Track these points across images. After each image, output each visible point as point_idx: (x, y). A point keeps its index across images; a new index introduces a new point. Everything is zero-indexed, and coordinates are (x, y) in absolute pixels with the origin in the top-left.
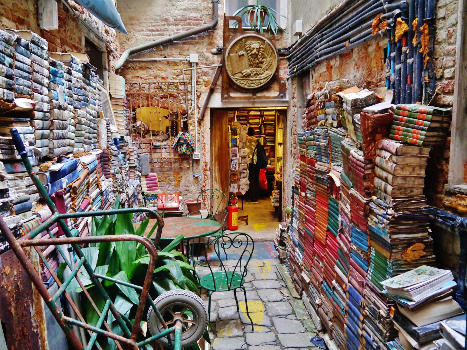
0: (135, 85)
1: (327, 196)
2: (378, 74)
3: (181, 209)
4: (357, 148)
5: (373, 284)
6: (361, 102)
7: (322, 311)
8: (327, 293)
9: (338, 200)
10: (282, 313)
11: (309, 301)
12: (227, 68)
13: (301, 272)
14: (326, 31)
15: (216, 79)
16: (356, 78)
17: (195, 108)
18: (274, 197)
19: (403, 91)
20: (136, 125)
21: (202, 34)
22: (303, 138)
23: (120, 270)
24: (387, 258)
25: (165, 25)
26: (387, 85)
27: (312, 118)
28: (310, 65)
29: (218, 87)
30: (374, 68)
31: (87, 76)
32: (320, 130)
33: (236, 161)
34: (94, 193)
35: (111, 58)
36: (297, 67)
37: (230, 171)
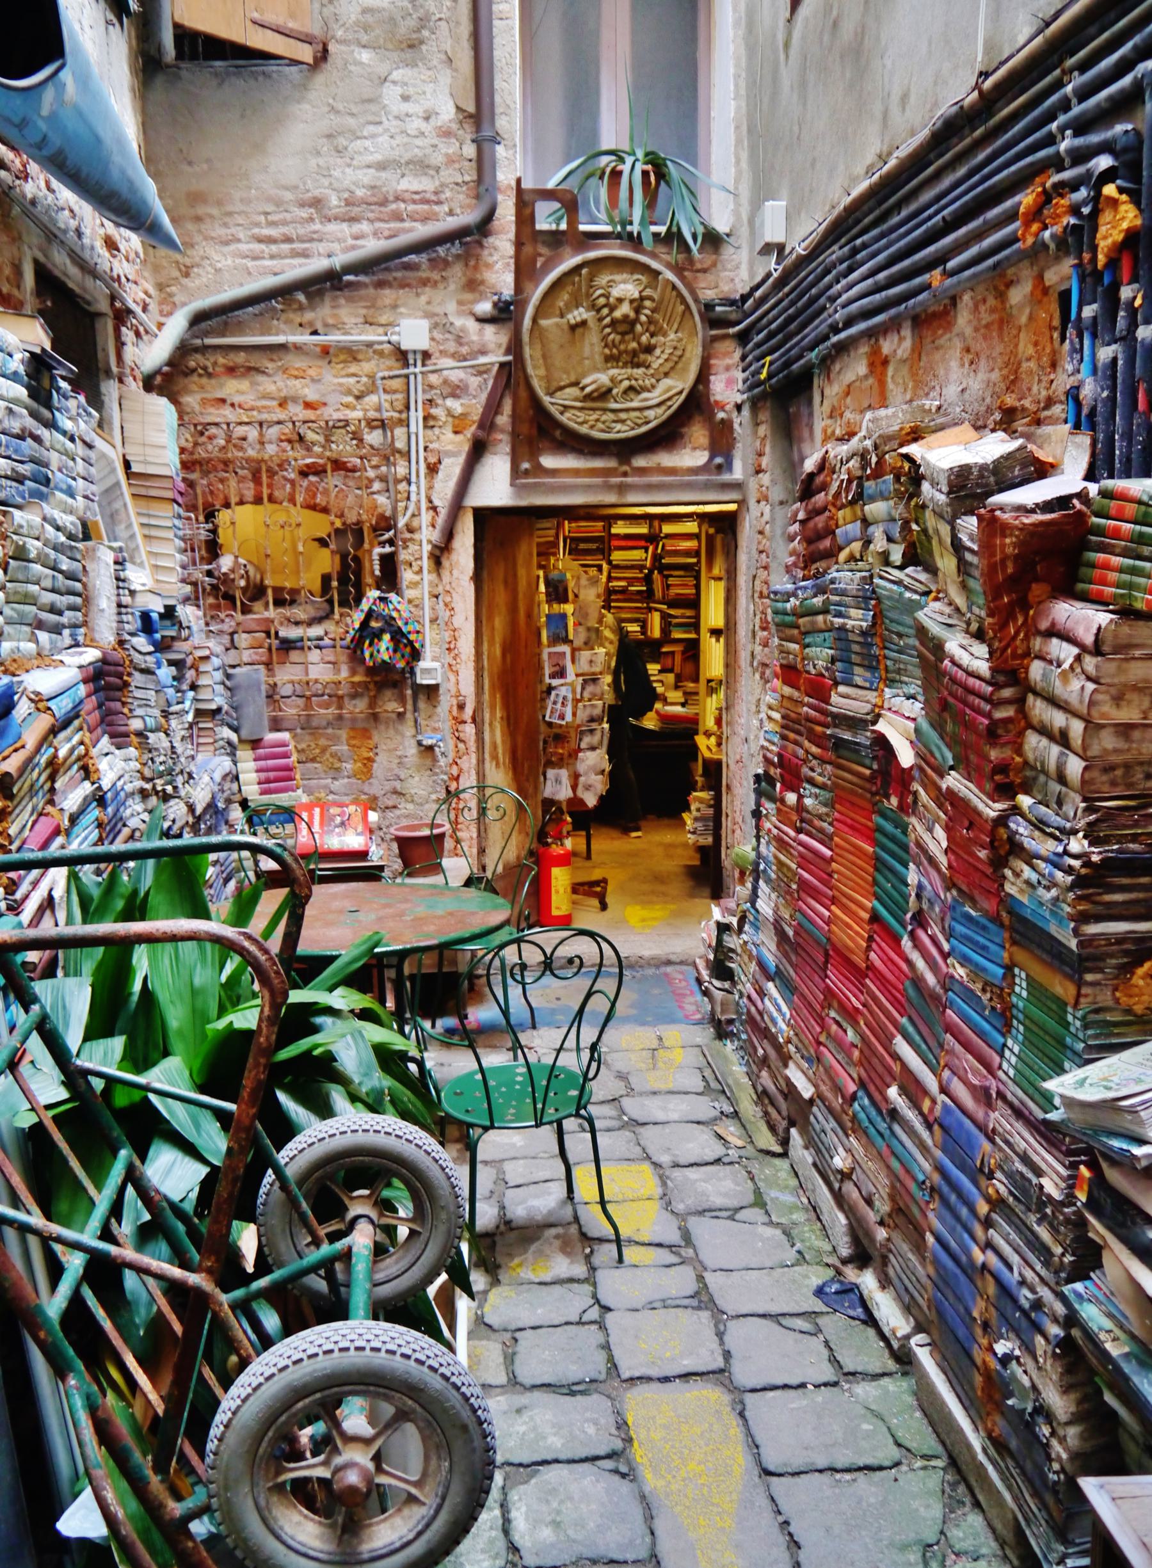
0: (213, 430)
1: (870, 801)
2: (1040, 381)
3: (377, 856)
4: (967, 632)
5: (1020, 1093)
6: (981, 476)
7: (855, 1194)
8: (872, 1130)
9: (908, 815)
10: (718, 1201)
11: (810, 1160)
12: (530, 370)
13: (786, 1066)
14: (865, 238)
15: (492, 407)
16: (966, 395)
17: (419, 509)
18: (695, 813)
19: (1122, 436)
20: (219, 567)
21: (441, 251)
22: (788, 606)
23: (166, 1053)
24: (1066, 1004)
25: (311, 219)
26: (1071, 417)
27: (819, 536)
28: (814, 354)
29: (500, 436)
30: (1029, 359)
31: (43, 393)
32: (844, 577)
33: (563, 691)
34: (73, 796)
35: (128, 335)
36: (771, 363)
37: (543, 728)
